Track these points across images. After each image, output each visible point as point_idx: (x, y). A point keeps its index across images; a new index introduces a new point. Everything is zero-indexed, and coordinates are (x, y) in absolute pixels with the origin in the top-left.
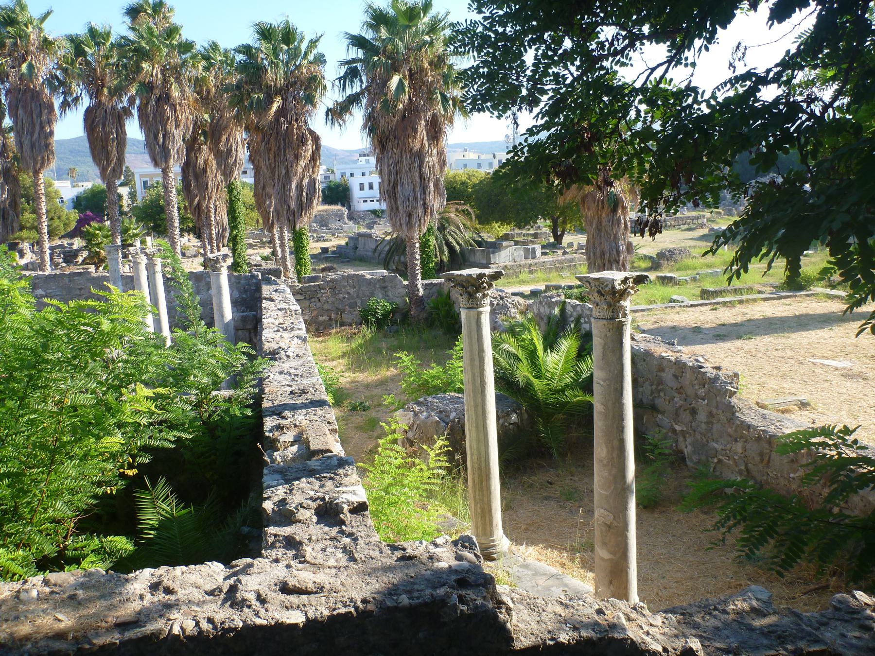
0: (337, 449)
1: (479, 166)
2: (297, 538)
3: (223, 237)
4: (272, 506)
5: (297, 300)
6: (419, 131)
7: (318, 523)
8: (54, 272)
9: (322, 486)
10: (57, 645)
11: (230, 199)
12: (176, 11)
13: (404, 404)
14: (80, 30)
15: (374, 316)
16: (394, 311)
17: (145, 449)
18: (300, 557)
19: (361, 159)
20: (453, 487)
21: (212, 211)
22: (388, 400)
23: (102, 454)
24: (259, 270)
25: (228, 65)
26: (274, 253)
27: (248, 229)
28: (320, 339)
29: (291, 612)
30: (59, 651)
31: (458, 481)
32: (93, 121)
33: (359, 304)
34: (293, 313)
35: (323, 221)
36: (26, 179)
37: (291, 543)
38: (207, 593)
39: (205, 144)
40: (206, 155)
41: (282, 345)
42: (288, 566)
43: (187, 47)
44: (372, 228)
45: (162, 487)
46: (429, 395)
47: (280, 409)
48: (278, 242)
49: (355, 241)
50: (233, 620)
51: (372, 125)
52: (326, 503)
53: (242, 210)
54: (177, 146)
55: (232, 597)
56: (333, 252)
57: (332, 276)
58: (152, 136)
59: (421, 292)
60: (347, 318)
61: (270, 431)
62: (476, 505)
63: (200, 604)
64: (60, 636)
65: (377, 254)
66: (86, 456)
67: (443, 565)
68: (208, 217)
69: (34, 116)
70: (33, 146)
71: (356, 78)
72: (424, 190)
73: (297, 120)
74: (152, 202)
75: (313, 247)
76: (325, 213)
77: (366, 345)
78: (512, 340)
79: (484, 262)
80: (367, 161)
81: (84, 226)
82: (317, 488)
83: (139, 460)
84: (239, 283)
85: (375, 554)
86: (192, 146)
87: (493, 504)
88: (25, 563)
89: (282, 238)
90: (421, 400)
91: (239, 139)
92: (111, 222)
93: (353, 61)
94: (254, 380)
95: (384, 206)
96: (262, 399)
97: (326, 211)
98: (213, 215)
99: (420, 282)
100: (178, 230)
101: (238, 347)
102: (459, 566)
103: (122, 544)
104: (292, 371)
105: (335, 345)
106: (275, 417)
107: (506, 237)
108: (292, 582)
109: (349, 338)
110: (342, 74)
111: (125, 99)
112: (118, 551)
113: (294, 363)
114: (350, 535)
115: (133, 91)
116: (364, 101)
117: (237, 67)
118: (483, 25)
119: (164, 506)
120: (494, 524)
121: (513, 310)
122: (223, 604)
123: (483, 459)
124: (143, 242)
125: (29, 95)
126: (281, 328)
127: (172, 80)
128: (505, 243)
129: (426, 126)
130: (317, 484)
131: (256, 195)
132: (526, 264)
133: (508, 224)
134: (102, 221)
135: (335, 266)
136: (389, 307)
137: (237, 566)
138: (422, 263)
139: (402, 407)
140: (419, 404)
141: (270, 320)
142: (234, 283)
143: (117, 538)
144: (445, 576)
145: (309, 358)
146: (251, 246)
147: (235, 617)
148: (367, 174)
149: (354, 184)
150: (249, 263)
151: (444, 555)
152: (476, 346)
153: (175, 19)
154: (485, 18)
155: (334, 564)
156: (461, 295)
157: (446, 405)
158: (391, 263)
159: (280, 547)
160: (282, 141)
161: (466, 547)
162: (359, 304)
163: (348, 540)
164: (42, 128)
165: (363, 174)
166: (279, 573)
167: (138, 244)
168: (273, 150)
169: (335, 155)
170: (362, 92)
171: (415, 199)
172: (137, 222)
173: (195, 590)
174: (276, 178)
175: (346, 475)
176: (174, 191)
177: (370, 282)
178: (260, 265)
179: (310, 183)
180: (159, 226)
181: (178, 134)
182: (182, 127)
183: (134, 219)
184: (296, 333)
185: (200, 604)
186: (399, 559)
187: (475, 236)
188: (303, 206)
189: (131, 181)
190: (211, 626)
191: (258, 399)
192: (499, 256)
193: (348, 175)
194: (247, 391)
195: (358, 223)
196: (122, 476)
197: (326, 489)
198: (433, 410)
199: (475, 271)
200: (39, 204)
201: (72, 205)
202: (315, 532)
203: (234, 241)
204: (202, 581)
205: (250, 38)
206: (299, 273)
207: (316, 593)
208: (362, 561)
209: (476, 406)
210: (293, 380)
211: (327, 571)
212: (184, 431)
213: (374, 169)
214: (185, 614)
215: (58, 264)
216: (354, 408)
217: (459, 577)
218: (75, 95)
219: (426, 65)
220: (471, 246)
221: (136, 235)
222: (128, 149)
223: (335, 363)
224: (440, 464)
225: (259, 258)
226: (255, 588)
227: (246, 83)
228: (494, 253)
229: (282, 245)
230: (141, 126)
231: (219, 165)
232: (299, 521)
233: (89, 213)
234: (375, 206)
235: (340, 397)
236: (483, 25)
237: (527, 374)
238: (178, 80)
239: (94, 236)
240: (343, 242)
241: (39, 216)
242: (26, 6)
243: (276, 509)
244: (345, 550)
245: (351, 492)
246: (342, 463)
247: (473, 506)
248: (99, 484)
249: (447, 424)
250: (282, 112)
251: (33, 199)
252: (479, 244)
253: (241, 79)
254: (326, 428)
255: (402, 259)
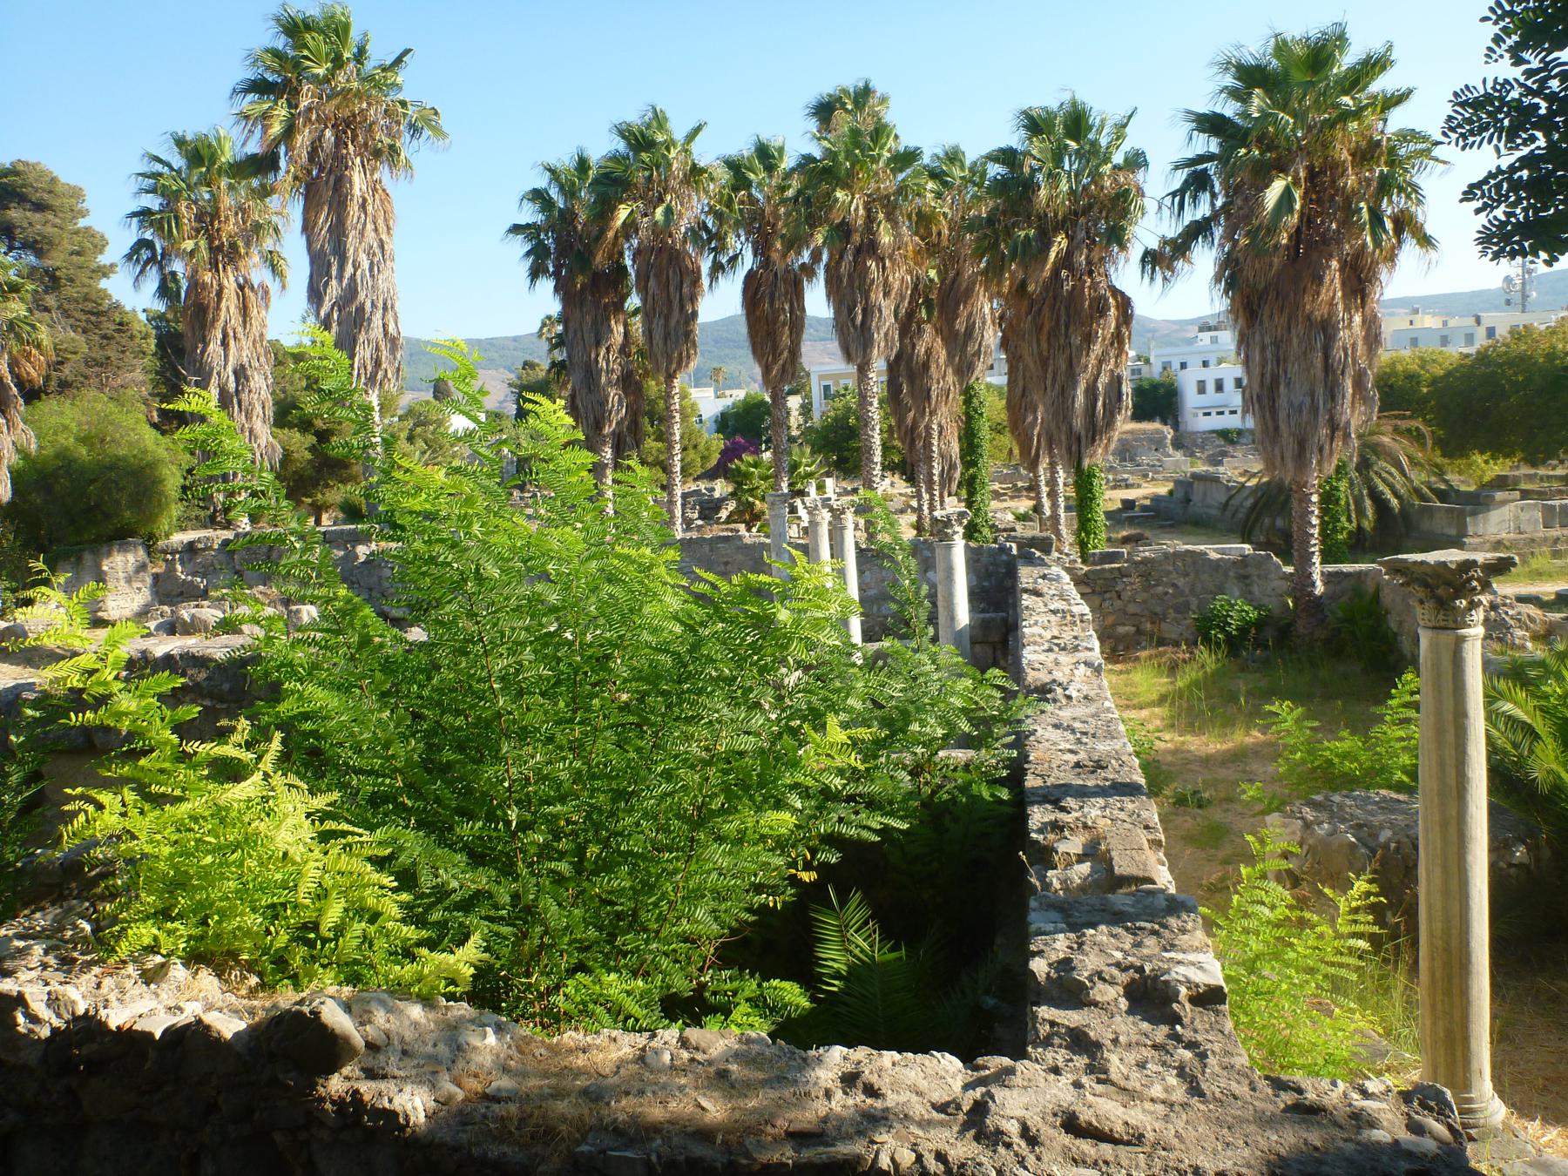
0: (1164, 878)
1: (1445, 341)
2: (1092, 1034)
3: (950, 479)
4: (1046, 969)
5: (1083, 595)
6: (1327, 279)
7: (1130, 1012)
8: (688, 535)
9: (1138, 945)
10: (699, 1150)
11: (967, 414)
12: (892, 103)
13: (1284, 803)
14: (741, 146)
15: (1223, 630)
16: (1260, 624)
17: (832, 840)
18: (1098, 1070)
19: (1201, 335)
20: (1382, 977)
21: (935, 435)
22: (1251, 791)
23: (763, 838)
24: (1013, 539)
25: (975, 184)
26: (1037, 509)
27: (991, 465)
28: (1118, 667)
29: (1082, 1170)
30: (701, 1160)
31: (1396, 968)
32: (756, 293)
33: (1194, 607)
34: (1077, 619)
35: (1126, 452)
36: (653, 387)
37: (1079, 1042)
38: (934, 1106)
39: (929, 320)
40: (929, 341)
41: (1058, 675)
42: (1077, 1085)
43: (907, 158)
44: (1220, 463)
45: (856, 911)
46: (1335, 790)
47: (1057, 793)
48: (1044, 489)
49: (1186, 488)
50: (980, 1164)
51: (1232, 274)
52: (1144, 978)
53: (985, 432)
54: (886, 324)
55: (977, 1121)
56: (1144, 508)
57: (1145, 552)
58: (845, 312)
59: (1319, 589)
60: (1170, 630)
61: (1040, 831)
62: (1434, 1023)
63: (925, 1124)
64: (704, 1134)
65: (1228, 514)
66: (740, 841)
67: (1380, 1135)
68: (928, 445)
69: (672, 289)
70: (666, 337)
71: (1205, 190)
72: (1333, 392)
73: (1090, 273)
74: (836, 419)
75: (1109, 499)
76: (1129, 437)
77: (1209, 684)
78: (1521, 695)
79: (1453, 532)
80: (1214, 340)
81: (731, 461)
82: (1127, 946)
83: (821, 856)
84: (978, 561)
85: (1242, 1090)
86: (908, 326)
87: (1473, 1027)
88: (644, 999)
89: (1052, 483)
90: (1319, 798)
91: (987, 310)
92: (775, 453)
93: (1201, 159)
94: (1009, 734)
95: (1250, 423)
96: (1024, 772)
97: (1131, 432)
98: (935, 442)
99: (1317, 569)
100: (879, 467)
101: (987, 676)
102: (1413, 1143)
103: (792, 994)
104: (1077, 725)
105: (1147, 680)
106: (1049, 807)
107: (1501, 483)
108: (1085, 1116)
109: (1173, 668)
110: (1177, 185)
111: (806, 257)
112: (785, 1006)
113: (1081, 711)
114: (1191, 1045)
115: (819, 239)
116: (1218, 232)
117: (989, 188)
118: (1521, 85)
119: (860, 941)
120: (1475, 1066)
121: (1519, 633)
122: (962, 1132)
123: (1455, 932)
124: (821, 488)
125: (665, 256)
126: (1055, 645)
127: (881, 216)
128: (1499, 496)
129: (1342, 270)
130: (1128, 940)
131: (1010, 406)
132: (1545, 539)
133: (1506, 456)
134: (757, 452)
135: (1148, 533)
136: (1253, 615)
137: (985, 1067)
138: (1323, 532)
139: (1278, 809)
140: (1315, 805)
141: (1036, 630)
142: (973, 558)
143: (787, 985)
144: (1385, 1159)
145: (1107, 704)
146: (997, 495)
147: (983, 1160)
148: (1212, 362)
149: (1187, 382)
150: (993, 526)
151: (1382, 1116)
152: (1449, 705)
153: (889, 117)
154: (1529, 73)
155: (1162, 1096)
156: (1421, 602)
157: (1371, 813)
158: (1257, 531)
159: (1060, 1046)
160: (1063, 312)
161: (1431, 1109)
162: (1194, 607)
163: (1188, 1054)
164: (682, 307)
165: (1205, 364)
166: (1061, 1095)
167: (812, 490)
168: (1046, 329)
169: (1154, 331)
170: (1215, 216)
171: (1314, 410)
172: (813, 453)
173: (914, 1098)
174: (1049, 376)
175: (1183, 931)
176: (876, 404)
177: (1216, 566)
178: (1013, 530)
179: (1109, 386)
180: (846, 460)
181: (887, 307)
182: (893, 295)
183: (808, 450)
184: (1083, 655)
185: (925, 1124)
186: (1288, 1109)
187: (1433, 479)
188: (1096, 429)
189: (804, 386)
190: (942, 1167)
191: (1017, 770)
192: (1486, 521)
193: (1176, 365)
194: (990, 758)
195: (1192, 455)
196: (794, 881)
197: (1145, 951)
198: (1343, 821)
199: (1452, 556)
200: (670, 427)
201: (714, 427)
202: (1124, 1028)
203: (971, 485)
204: (925, 1083)
205: (1013, 138)
206: (1083, 545)
207: (1128, 1143)
208: (1215, 1099)
209: (1444, 824)
210: (1079, 741)
211: (1148, 1105)
212: (892, 814)
213: (1233, 354)
214: (897, 1137)
215: (692, 521)
216: (1181, 801)
217: (1416, 1167)
218: (731, 253)
219: (1345, 156)
220: (1423, 498)
221: (810, 475)
222: (808, 333)
223: (1145, 713)
224: (1360, 928)
225: (1010, 517)
226: (1020, 1113)
227: (1004, 213)
228: (1474, 514)
229: (1053, 495)
230: (828, 296)
231: (950, 356)
232: (1096, 1004)
233: (738, 438)
234: (1232, 422)
235: (1158, 775)
236: (1521, 85)
237: (1554, 766)
238: (890, 217)
239: (748, 476)
240: (1163, 490)
241: (670, 447)
242: (666, 119)
243: (1053, 974)
244: (1181, 1072)
245: (1193, 964)
246: (1175, 906)
247: (1428, 1023)
248: (758, 889)
249: (1374, 852)
250: (1066, 261)
251: (662, 419)
252: (1442, 496)
253: (996, 208)
254: (1143, 837)
255: (1280, 523)
